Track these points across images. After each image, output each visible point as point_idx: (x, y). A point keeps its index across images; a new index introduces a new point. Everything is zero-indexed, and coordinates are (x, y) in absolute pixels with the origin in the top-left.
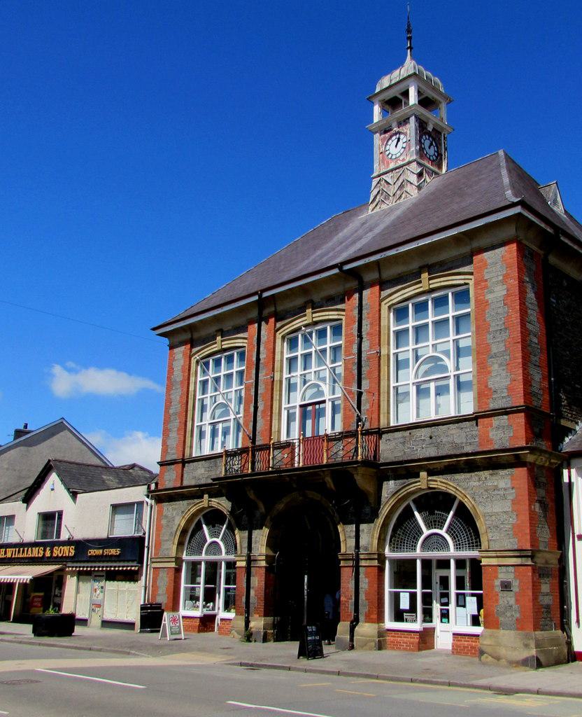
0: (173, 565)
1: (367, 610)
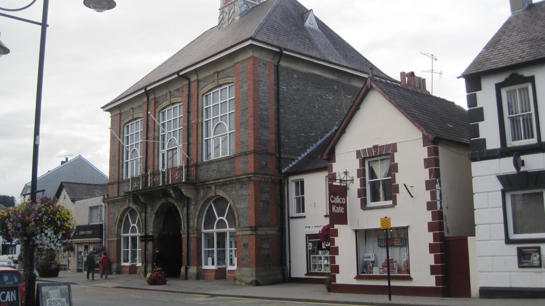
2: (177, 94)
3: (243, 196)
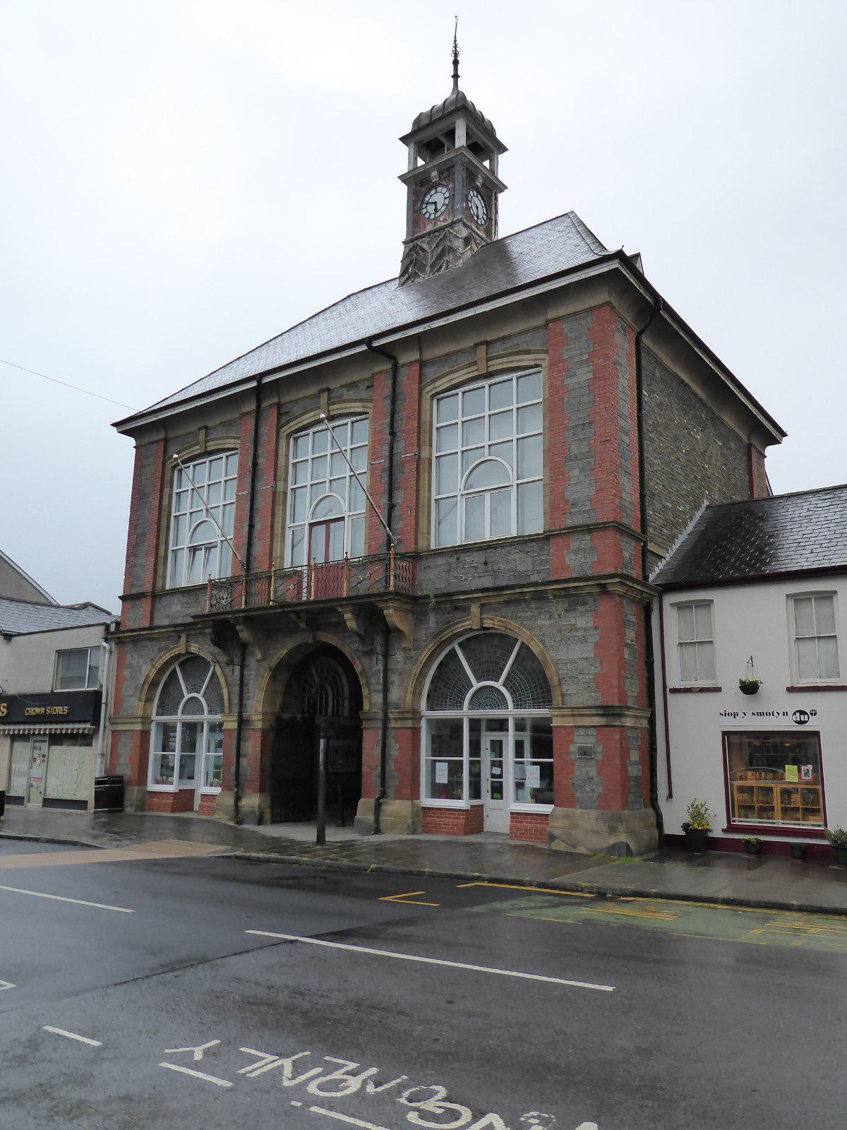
0: (139, 727)
2: (348, 394)
3: (577, 630)
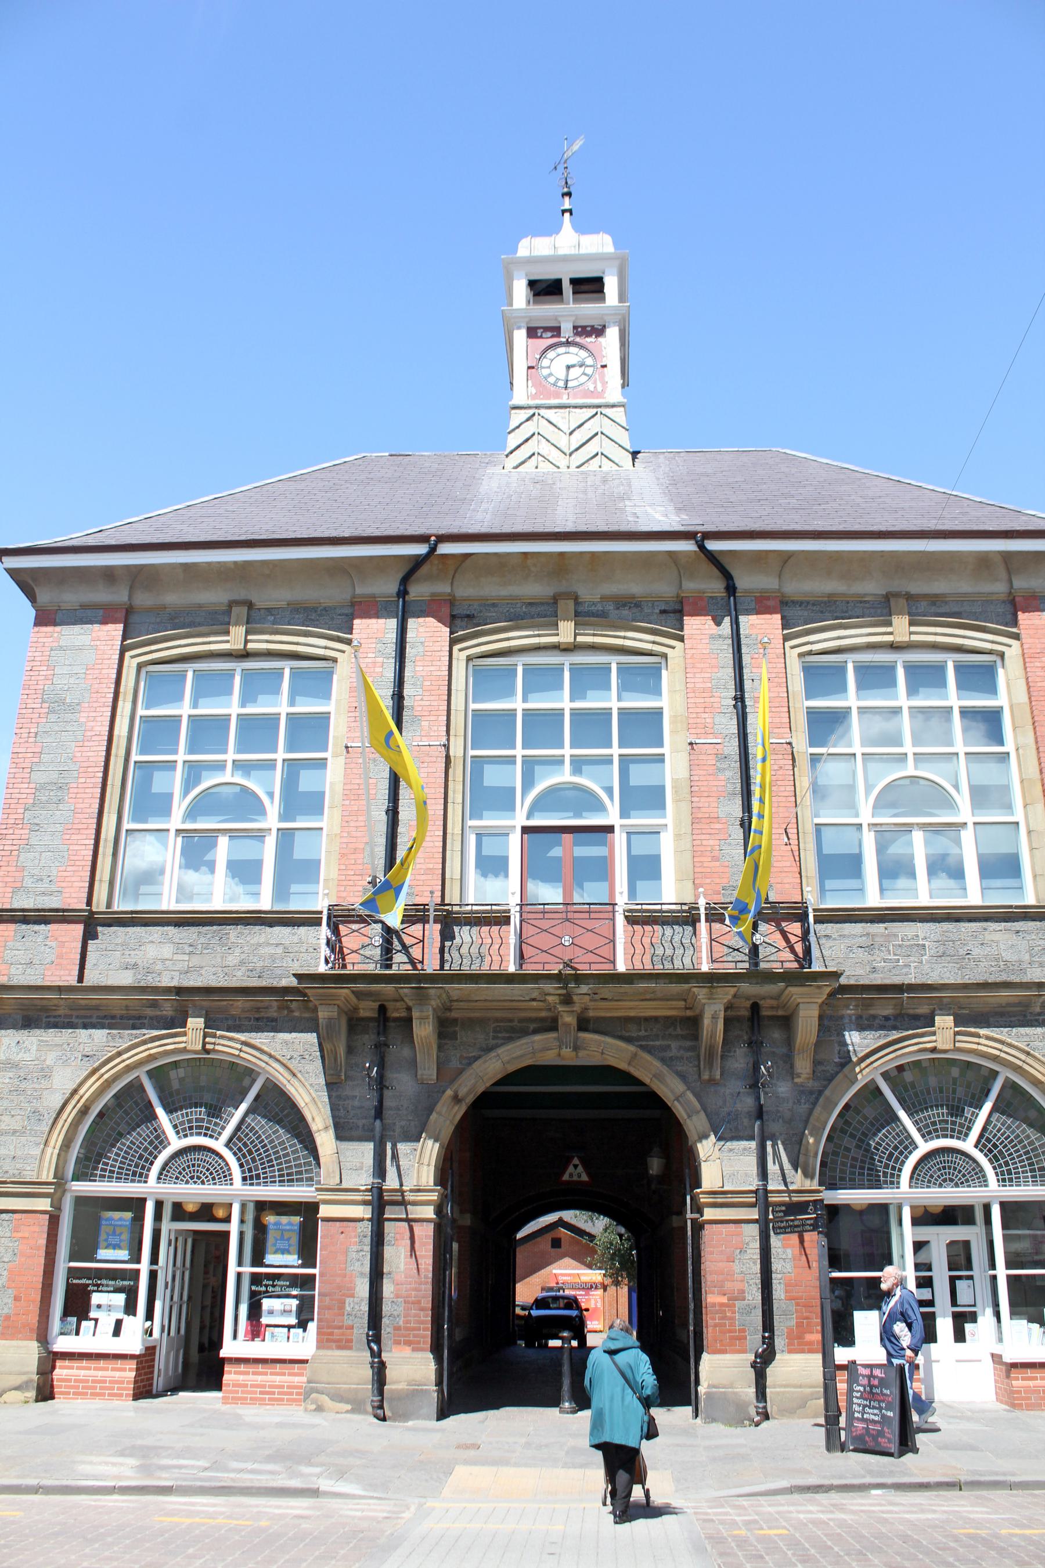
0: (45, 1204)
1: (793, 1323)
